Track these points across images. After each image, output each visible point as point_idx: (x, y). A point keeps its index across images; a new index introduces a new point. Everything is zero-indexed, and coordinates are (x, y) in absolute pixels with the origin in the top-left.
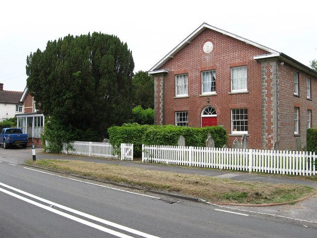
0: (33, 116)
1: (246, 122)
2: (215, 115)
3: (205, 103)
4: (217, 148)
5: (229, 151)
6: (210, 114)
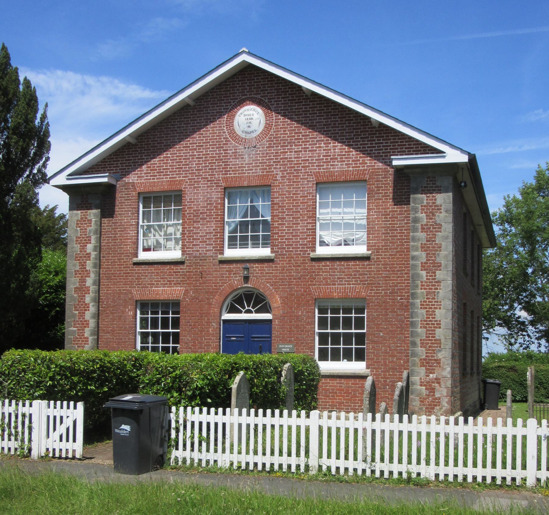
2: (267, 316)
3: (237, 282)
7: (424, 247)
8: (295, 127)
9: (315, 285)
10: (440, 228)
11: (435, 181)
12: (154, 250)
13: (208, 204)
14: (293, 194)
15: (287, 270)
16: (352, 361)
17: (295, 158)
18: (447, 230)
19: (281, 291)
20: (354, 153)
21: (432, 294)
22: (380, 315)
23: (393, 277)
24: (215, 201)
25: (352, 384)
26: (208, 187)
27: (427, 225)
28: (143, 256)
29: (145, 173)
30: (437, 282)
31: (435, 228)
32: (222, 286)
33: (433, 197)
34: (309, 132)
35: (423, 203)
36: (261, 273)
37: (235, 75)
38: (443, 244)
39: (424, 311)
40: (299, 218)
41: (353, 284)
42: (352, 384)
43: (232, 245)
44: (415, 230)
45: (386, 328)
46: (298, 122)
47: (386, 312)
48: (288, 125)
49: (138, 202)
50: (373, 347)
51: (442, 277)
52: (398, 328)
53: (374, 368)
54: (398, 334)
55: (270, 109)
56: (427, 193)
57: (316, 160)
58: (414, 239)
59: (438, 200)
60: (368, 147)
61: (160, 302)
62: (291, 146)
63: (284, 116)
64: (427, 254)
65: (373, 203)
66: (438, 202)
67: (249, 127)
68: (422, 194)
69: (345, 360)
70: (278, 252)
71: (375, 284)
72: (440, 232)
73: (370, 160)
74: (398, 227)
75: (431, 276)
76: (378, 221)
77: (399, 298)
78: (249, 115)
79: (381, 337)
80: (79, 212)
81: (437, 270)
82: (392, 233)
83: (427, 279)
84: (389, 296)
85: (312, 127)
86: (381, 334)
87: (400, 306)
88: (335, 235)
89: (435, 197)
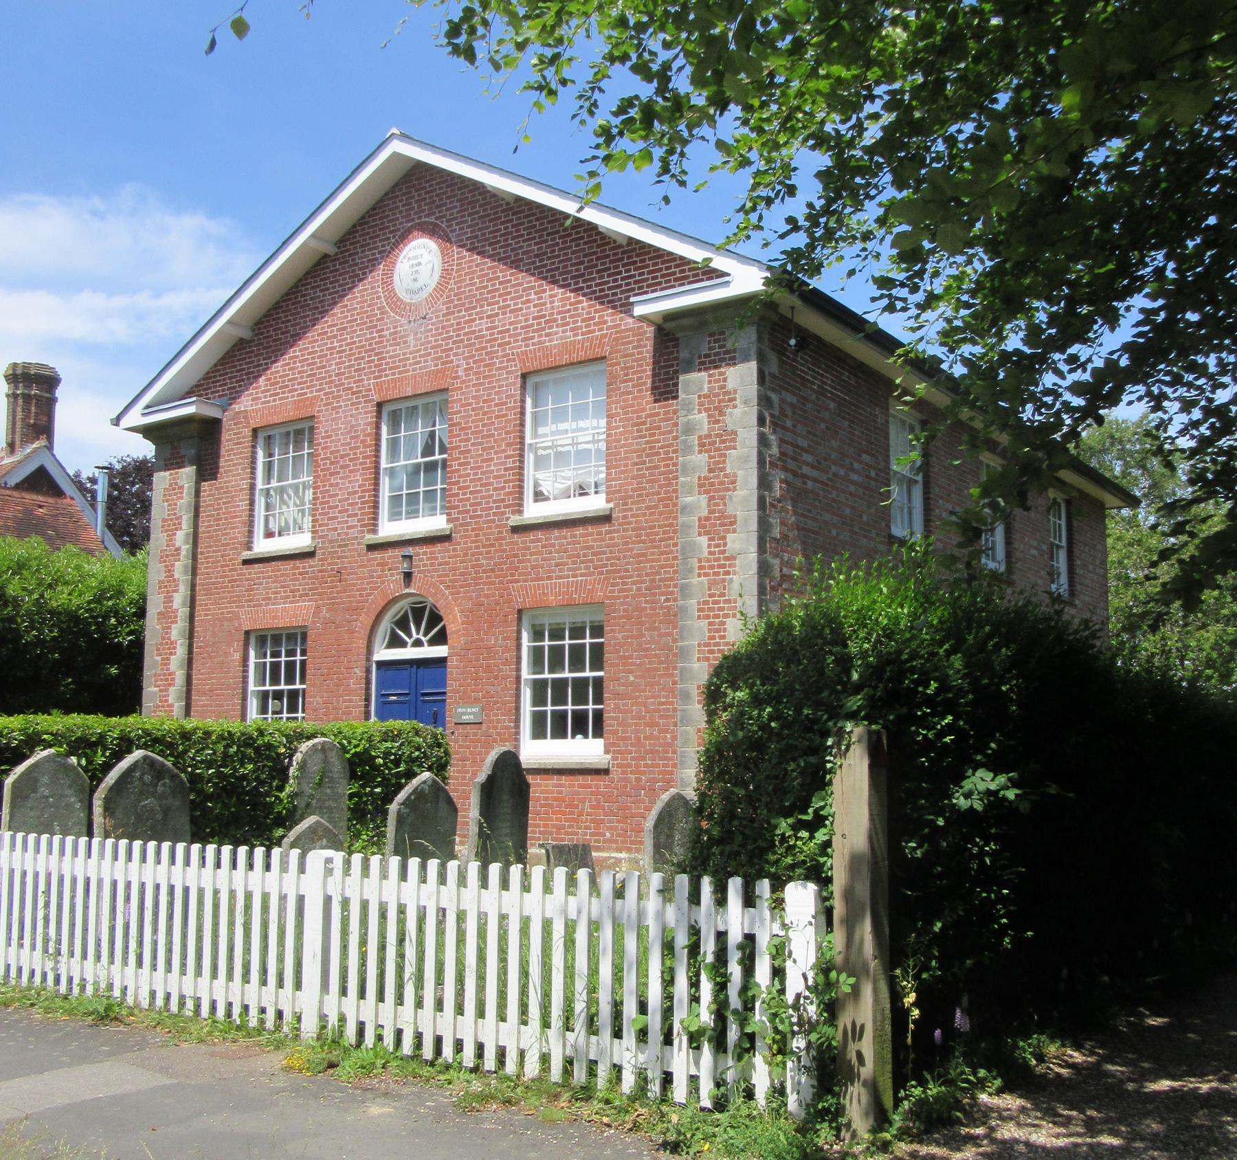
0: (291, 482)
1: (598, 682)
2: (440, 651)
3: (394, 584)
4: (495, 869)
5: (403, 876)
6: (418, 643)
7: (704, 485)
8: (489, 268)
9: (517, 581)
10: (734, 440)
11: (725, 340)
12: (280, 535)
13: (352, 438)
14: (484, 401)
15: (472, 555)
16: (545, 737)
17: (488, 329)
18: (747, 442)
19: (463, 598)
20: (585, 304)
21: (718, 583)
22: (628, 637)
23: (653, 554)
24: (364, 430)
25: (581, 786)
26: (352, 404)
27: (709, 436)
28: (263, 546)
29: (263, 392)
30: (727, 559)
31: (723, 442)
32: (369, 595)
33: (721, 374)
34: (511, 275)
35: (701, 389)
36: (432, 564)
37: (397, 185)
38: (740, 473)
39: (704, 623)
40: (493, 447)
41: (582, 575)
42: (581, 786)
43: (395, 515)
44: (687, 450)
45: (640, 665)
46: (492, 257)
47: (640, 630)
48: (477, 266)
49: (254, 447)
50: (617, 706)
51: (737, 546)
52: (661, 662)
53: (619, 752)
54: (661, 676)
55: (449, 241)
56: (709, 368)
57: (522, 328)
58: (685, 471)
59: (729, 380)
60: (609, 289)
61: (284, 632)
62: (482, 306)
63: (471, 250)
64: (712, 498)
65: (617, 402)
66: (730, 385)
67: (415, 280)
68: (700, 370)
69: (579, 736)
70: (457, 519)
71: (619, 571)
72: (735, 448)
73: (613, 314)
74: (661, 448)
75: (717, 546)
76: (626, 439)
77: (663, 598)
78: (416, 257)
79: (631, 684)
80: (167, 473)
81: (728, 531)
82: (650, 461)
83: (710, 553)
84: (645, 595)
85: (515, 264)
86: (632, 679)
87: (665, 614)
88: (564, 478)
89: (724, 373)
